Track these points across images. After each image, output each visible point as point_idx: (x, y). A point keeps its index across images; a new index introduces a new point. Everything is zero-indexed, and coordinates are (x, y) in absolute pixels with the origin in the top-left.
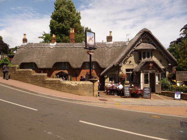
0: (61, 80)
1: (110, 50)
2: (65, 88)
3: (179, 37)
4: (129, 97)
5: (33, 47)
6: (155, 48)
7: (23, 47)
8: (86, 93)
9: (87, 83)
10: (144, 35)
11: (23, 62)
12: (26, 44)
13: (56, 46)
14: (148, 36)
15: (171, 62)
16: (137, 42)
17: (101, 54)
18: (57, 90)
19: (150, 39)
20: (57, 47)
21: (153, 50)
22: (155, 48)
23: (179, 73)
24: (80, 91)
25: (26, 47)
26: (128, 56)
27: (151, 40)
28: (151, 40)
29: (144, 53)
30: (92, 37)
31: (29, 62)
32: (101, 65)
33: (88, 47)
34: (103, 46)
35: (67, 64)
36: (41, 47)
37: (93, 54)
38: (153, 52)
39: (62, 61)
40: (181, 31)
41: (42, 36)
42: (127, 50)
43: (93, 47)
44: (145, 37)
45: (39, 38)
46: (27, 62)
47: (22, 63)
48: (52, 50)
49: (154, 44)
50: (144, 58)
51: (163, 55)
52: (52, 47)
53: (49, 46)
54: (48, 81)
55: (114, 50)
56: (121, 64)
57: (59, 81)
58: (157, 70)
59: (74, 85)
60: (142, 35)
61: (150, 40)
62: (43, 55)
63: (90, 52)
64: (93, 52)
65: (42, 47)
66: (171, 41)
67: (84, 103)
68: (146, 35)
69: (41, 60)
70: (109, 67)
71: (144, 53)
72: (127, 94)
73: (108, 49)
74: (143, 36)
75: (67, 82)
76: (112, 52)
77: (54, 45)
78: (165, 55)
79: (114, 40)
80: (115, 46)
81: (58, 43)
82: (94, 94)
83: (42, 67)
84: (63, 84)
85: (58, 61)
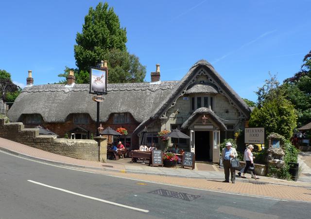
0: (55, 138)
1: (153, 95)
2: (59, 149)
3: (298, 70)
4: (160, 166)
5: (41, 90)
6: (215, 91)
7: (27, 90)
8: (86, 156)
9: (90, 142)
10: (200, 70)
11: (24, 112)
12: (31, 85)
13: (74, 90)
14: (206, 72)
15: (242, 114)
16: (190, 82)
17: (138, 101)
18: (49, 151)
19: (209, 76)
20: (75, 90)
21: (213, 94)
22: (215, 91)
23: (248, 131)
24: (77, 153)
25: (30, 91)
26: (173, 104)
27: (211, 78)
28: (210, 77)
29: (199, 99)
30: (102, 77)
31: (32, 112)
32: (136, 117)
33: (92, 91)
34: (144, 89)
35: (128, 114)
36: (52, 90)
37: (102, 101)
38: (215, 98)
39: (79, 112)
40: (305, 60)
41: (63, 73)
42: (171, 95)
43: (102, 91)
44: (200, 74)
45: (59, 76)
46: (29, 113)
47: (23, 115)
48: (67, 95)
49: (216, 84)
50: (199, 106)
51: (230, 102)
52: (67, 91)
53: (64, 90)
54: (39, 138)
55: (161, 95)
56: (163, 117)
57: (52, 138)
58: (216, 126)
59: (70, 144)
60: (195, 71)
61: (209, 79)
62: (53, 103)
63: (97, 99)
64: (101, 98)
65: (54, 90)
66: (286, 79)
67: (84, 170)
68: (202, 71)
69: (50, 110)
70: (144, 122)
71: (199, 99)
72: (156, 161)
73: (151, 93)
74: (198, 72)
75: (62, 141)
76: (156, 98)
77: (71, 87)
78: (232, 101)
79: (36, 83)
80: (164, 88)
81: (77, 85)
82: (99, 159)
83: (49, 121)
84: (56, 143)
85: (73, 112)
